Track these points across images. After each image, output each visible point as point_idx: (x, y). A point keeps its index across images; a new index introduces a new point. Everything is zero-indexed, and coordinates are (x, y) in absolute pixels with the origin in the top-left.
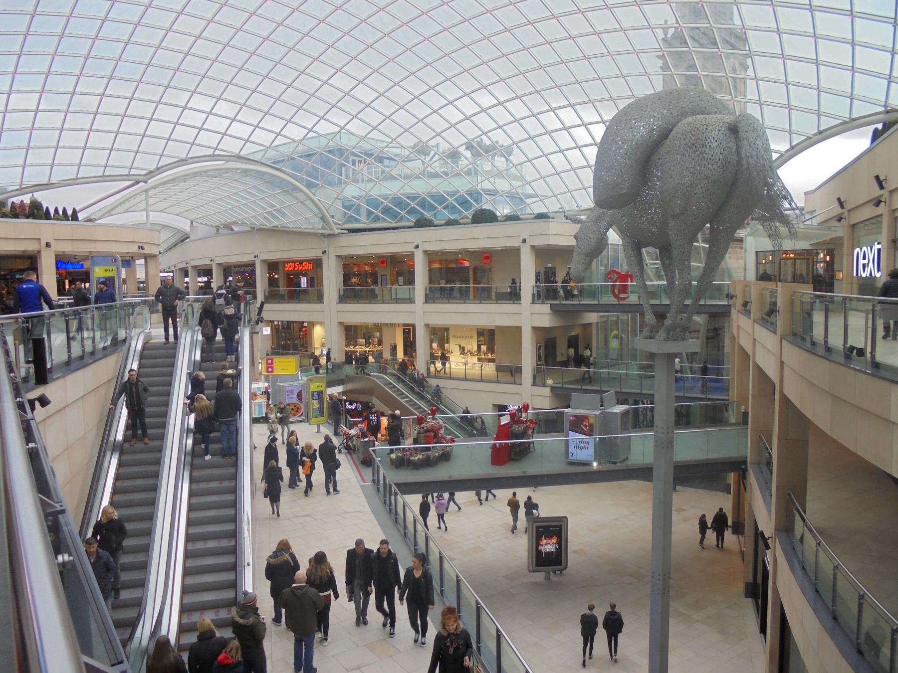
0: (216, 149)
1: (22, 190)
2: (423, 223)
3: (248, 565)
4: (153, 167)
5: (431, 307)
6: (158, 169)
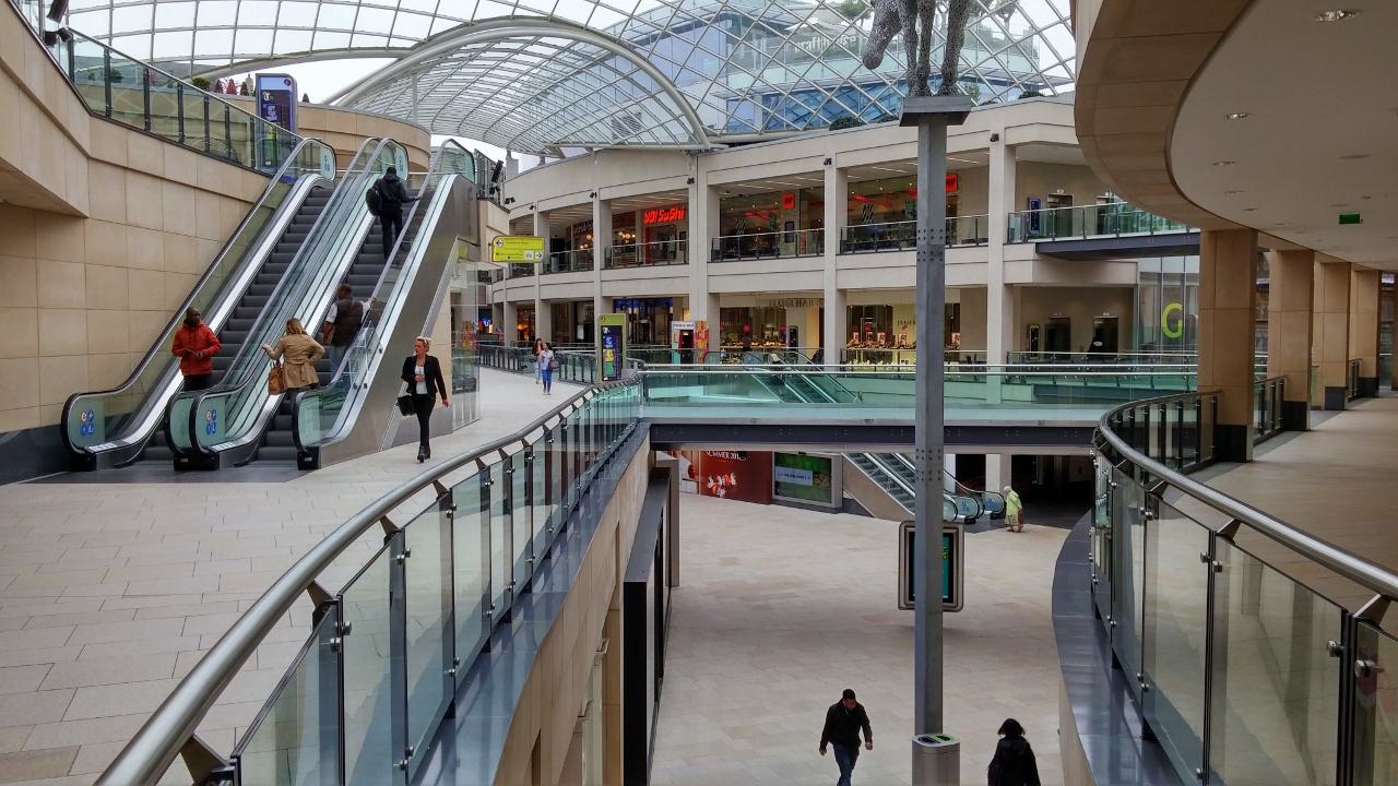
0: (390, 36)
1: (235, 68)
2: (842, 123)
3: (381, 351)
4: (423, 36)
5: (852, 260)
6: (430, 39)
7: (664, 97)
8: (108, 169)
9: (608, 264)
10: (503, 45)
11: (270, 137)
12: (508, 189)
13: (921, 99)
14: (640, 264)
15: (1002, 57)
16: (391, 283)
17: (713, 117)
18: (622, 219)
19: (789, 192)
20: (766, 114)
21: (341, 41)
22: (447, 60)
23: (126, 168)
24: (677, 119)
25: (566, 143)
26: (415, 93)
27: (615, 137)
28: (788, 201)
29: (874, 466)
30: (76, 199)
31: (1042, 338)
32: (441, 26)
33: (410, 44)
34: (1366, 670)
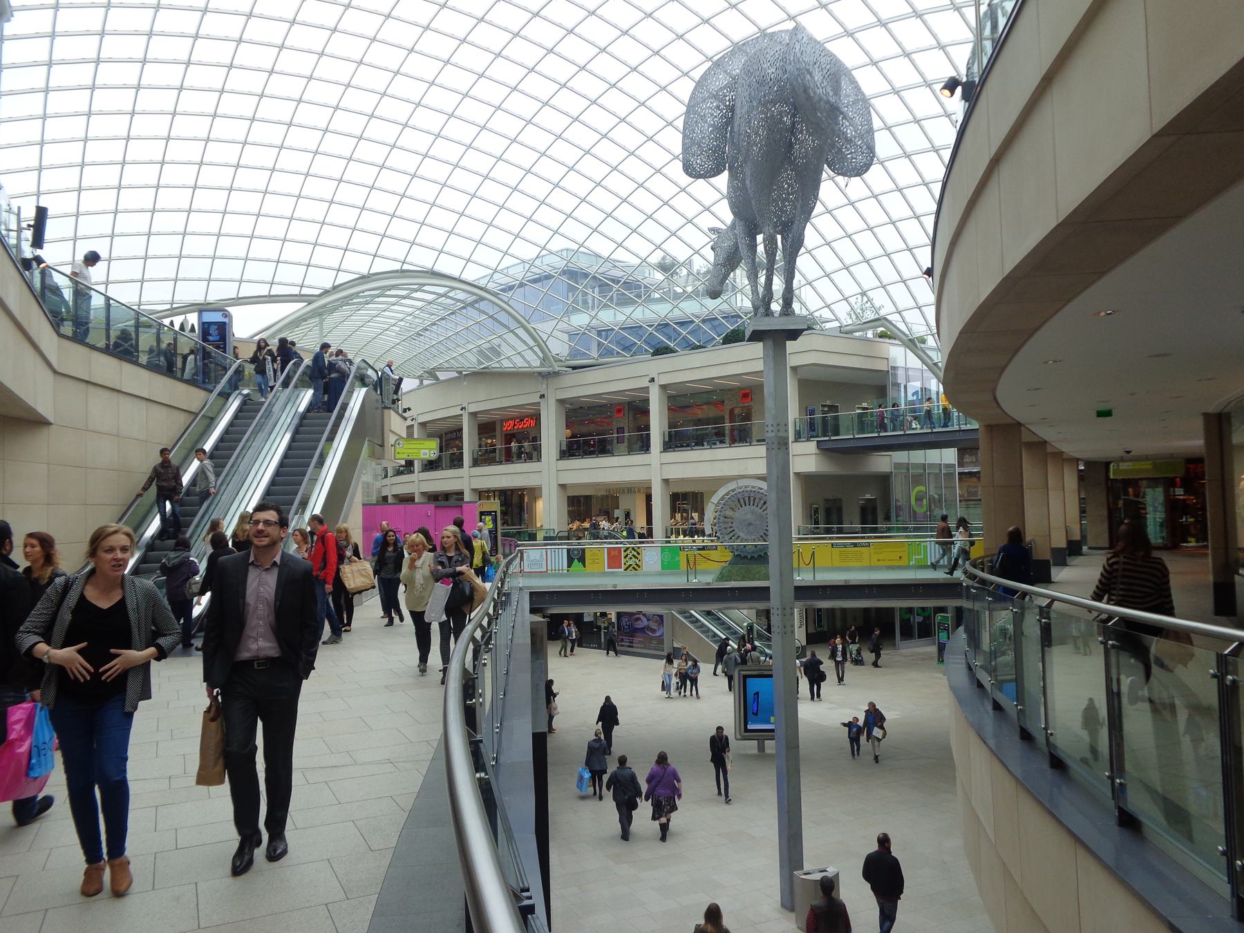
1: (173, 312)
2: (661, 351)
4: (329, 286)
6: (334, 288)
7: (521, 332)
8: (71, 383)
9: (476, 463)
10: (393, 292)
12: (404, 403)
13: (767, 319)
14: (500, 463)
16: (314, 480)
17: (559, 347)
18: (486, 428)
19: (620, 404)
20: (600, 344)
21: (263, 290)
22: (348, 304)
23: (87, 382)
24: (531, 348)
25: (440, 368)
26: (321, 329)
27: (480, 363)
28: (619, 411)
29: (698, 620)
30: (44, 408)
31: (821, 516)
32: (343, 278)
33: (318, 292)
34: (1121, 784)
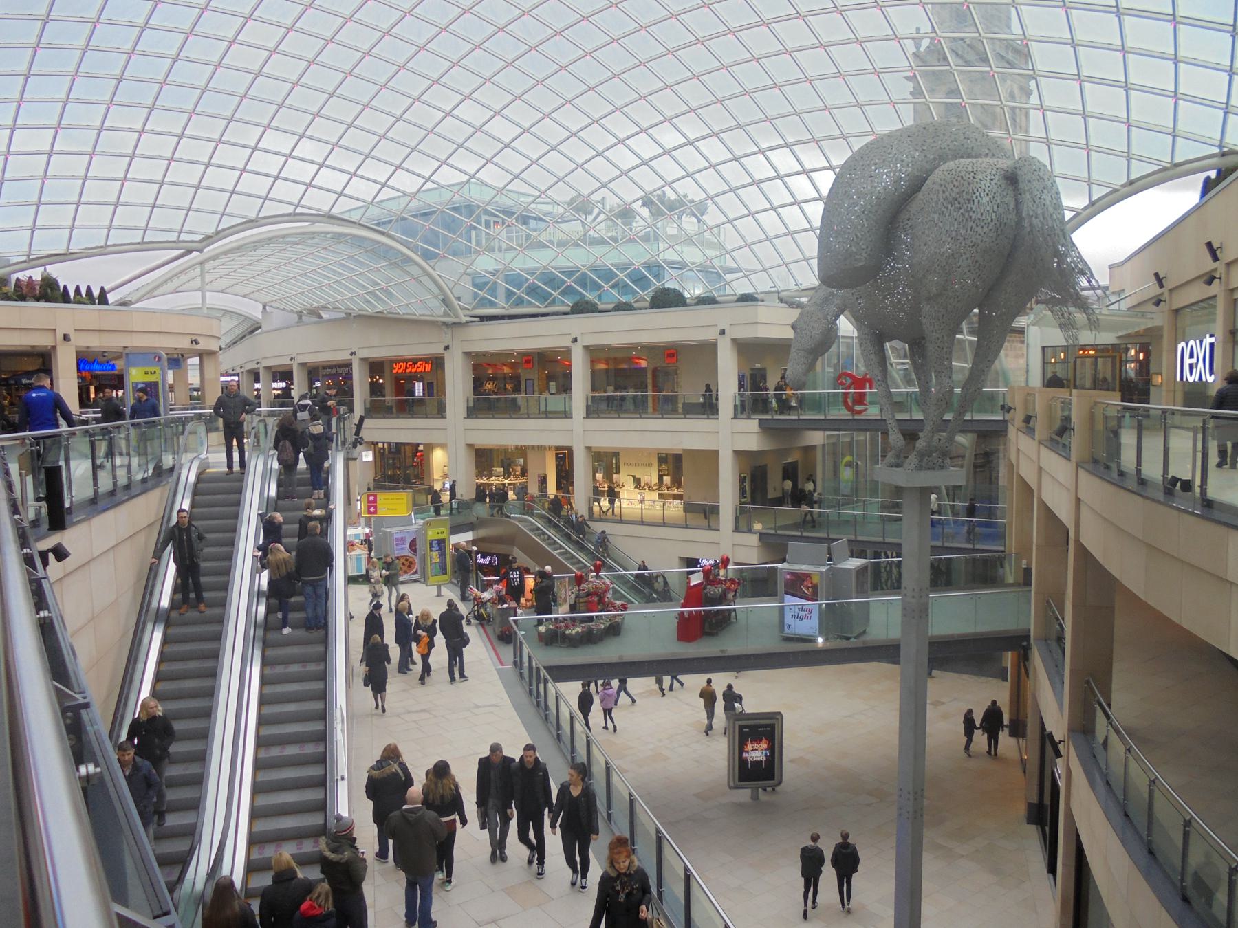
0: (298, 206)
1: (30, 262)
2: (582, 308)
4: (210, 231)
5: (595, 423)
6: (217, 233)
11: (118, 461)
15: (678, 248)
